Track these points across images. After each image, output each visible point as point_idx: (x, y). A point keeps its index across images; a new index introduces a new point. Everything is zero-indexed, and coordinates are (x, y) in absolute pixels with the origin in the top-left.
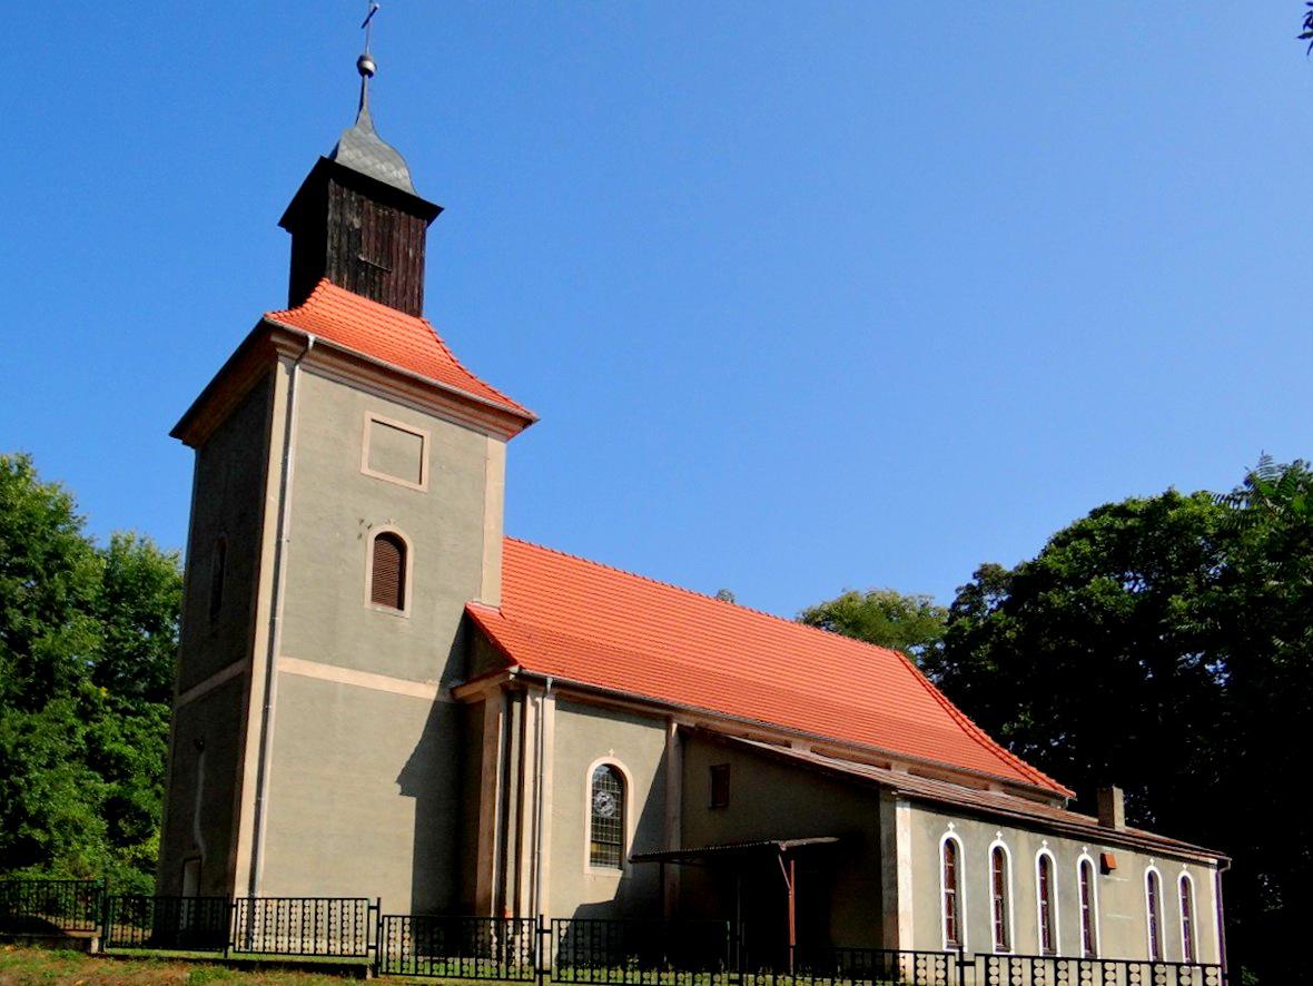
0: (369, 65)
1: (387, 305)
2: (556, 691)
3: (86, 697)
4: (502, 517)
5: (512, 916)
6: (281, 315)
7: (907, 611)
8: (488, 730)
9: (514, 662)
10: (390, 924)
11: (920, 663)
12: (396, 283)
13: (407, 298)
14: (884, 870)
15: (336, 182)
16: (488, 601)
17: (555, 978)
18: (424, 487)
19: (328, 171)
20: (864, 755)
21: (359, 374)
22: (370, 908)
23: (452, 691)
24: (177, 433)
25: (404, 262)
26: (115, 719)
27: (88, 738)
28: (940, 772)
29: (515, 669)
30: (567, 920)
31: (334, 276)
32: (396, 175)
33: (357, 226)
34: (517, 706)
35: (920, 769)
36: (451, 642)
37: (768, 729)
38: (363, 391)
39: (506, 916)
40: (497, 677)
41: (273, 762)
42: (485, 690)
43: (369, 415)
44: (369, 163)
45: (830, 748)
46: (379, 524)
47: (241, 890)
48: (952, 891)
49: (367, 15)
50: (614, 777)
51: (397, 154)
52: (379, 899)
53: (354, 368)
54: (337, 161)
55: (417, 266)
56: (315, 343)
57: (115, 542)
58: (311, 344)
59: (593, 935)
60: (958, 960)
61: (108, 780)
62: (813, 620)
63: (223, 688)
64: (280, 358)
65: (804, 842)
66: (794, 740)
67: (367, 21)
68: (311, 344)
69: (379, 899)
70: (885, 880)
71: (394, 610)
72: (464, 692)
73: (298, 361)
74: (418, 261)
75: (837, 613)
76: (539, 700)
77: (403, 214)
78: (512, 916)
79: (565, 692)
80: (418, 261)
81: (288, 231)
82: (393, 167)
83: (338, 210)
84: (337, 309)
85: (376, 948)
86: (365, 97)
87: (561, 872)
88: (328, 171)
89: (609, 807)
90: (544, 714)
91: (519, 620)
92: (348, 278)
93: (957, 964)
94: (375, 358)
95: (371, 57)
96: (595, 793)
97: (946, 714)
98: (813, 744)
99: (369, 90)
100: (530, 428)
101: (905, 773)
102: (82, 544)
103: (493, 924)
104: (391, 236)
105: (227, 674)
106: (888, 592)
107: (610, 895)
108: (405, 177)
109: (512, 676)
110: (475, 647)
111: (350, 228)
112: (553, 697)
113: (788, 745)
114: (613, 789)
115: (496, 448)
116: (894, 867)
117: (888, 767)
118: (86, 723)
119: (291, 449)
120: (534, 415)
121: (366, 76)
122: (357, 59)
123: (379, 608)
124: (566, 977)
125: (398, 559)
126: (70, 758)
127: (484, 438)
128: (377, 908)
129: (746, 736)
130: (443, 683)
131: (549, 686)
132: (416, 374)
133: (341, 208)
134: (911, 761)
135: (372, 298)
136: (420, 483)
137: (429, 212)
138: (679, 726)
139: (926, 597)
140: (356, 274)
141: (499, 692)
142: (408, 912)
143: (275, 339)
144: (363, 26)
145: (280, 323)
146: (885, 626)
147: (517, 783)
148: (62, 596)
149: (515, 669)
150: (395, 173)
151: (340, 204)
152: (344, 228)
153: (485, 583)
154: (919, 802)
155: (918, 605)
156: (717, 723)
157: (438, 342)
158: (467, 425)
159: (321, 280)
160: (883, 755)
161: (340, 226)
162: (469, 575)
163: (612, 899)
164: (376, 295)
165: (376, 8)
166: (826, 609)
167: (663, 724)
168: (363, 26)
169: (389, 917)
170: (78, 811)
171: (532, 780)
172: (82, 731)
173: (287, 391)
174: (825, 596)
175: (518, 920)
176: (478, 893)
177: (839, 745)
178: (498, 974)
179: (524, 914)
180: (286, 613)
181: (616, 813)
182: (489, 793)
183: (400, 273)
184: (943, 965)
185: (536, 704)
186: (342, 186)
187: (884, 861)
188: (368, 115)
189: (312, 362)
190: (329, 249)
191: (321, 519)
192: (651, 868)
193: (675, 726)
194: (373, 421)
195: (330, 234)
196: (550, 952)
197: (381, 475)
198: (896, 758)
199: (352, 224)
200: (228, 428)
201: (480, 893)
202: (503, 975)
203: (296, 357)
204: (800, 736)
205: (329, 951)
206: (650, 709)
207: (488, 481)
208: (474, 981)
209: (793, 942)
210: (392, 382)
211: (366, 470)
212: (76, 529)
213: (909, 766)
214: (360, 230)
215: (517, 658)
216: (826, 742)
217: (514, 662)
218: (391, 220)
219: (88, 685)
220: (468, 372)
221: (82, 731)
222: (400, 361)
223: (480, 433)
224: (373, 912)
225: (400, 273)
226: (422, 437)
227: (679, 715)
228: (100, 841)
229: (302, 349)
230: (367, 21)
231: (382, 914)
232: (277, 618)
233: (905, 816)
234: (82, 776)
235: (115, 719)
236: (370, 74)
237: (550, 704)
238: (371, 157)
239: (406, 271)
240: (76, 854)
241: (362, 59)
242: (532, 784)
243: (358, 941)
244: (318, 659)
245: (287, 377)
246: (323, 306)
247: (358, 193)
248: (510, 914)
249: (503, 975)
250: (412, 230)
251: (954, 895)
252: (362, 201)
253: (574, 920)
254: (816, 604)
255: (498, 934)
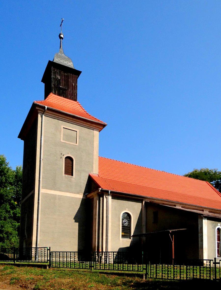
0: (62, 36)
1: (68, 99)
2: (111, 194)
3: (12, 204)
4: (98, 151)
5: (101, 251)
6: (38, 102)
7: (211, 173)
8: (94, 205)
9: (100, 187)
10: (52, 254)
11: (214, 185)
12: (70, 92)
13: (73, 96)
14: (199, 237)
15: (53, 67)
16: (95, 172)
17: (95, 268)
18: (77, 144)
19: (52, 65)
20: (196, 208)
21: (59, 116)
22: (48, 250)
23: (86, 196)
24: (19, 137)
25: (72, 87)
26: (19, 209)
27: (13, 213)
28: (218, 212)
29: (100, 189)
30: (116, 252)
31: (54, 92)
32: (70, 64)
33: (59, 78)
34: (101, 198)
35: (211, 211)
36: (86, 183)
37: (169, 202)
38: (61, 121)
39: (100, 251)
40: (96, 191)
41: (41, 215)
42: (93, 194)
43: (63, 126)
44: (62, 62)
45: (187, 206)
46: (66, 154)
47: (34, 246)
48: (219, 242)
49: (61, 23)
50: (128, 216)
51: (70, 59)
52: (50, 247)
53: (58, 114)
54: (54, 62)
55: (75, 88)
56: (47, 108)
57: (17, 168)
58: (46, 109)
59: (123, 255)
60: (214, 262)
61: (18, 223)
62: (186, 176)
63: (29, 197)
64: (39, 113)
65: (177, 230)
66: (177, 204)
67: (61, 25)
68: (46, 109)
69: (50, 247)
70: (200, 239)
71: (71, 176)
72: (89, 196)
73: (43, 114)
74: (75, 86)
75: (192, 175)
76: (107, 197)
77: (71, 74)
78: (101, 251)
79: (114, 194)
80: (75, 86)
81: (44, 83)
82: (68, 62)
83: (54, 75)
84: (55, 100)
85: (49, 260)
86: (61, 45)
87: (114, 240)
88: (52, 65)
89: (127, 223)
90: (109, 201)
91: (103, 177)
92: (57, 92)
93: (213, 263)
94: (63, 111)
95: (62, 34)
96: (123, 220)
97: (210, 186)
98: (182, 205)
99: (62, 43)
100: (106, 127)
101: (208, 212)
102: (8, 169)
103: (96, 253)
104: (68, 81)
105: (30, 194)
106: (206, 169)
107: (128, 245)
108: (72, 65)
109: (100, 191)
110: (91, 185)
111: (60, 79)
112: (111, 196)
113: (175, 206)
114: (128, 218)
115: (96, 133)
116: (202, 236)
117: (203, 211)
118: (13, 210)
119: (42, 136)
120: (106, 123)
121: (61, 39)
122: (59, 35)
123: (67, 176)
124: (98, 268)
125: (71, 163)
126: (9, 218)
127: (93, 131)
128: (50, 250)
129: (164, 204)
130: (84, 194)
131: (109, 193)
132: (74, 115)
133: (55, 73)
134: (210, 209)
135: (64, 97)
136: (76, 143)
137: (78, 73)
138: (145, 202)
139: (216, 169)
140: (60, 91)
141: (97, 195)
142: (77, 250)
143: (37, 108)
144: (60, 26)
145: (38, 104)
146: (204, 177)
147: (102, 218)
148: (4, 180)
149: (100, 189)
150: (69, 64)
151: (55, 73)
152: (56, 79)
153: (94, 168)
154: (209, 218)
155: (214, 172)
156: (155, 201)
157: (81, 107)
158: (89, 128)
159: (50, 93)
160: (201, 207)
161: (55, 79)
162: (90, 165)
163: (129, 246)
164: (65, 96)
165: (63, 20)
166: (189, 174)
167: (141, 202)
168: (60, 26)
169: (52, 252)
170: (10, 230)
171: (106, 217)
172: (12, 212)
173: (41, 122)
174: (190, 171)
175: (102, 252)
176: (93, 245)
177: (189, 205)
178: (80, 267)
179: (104, 250)
180: (42, 178)
181: (128, 225)
182: (95, 221)
183: (71, 90)
184: (209, 264)
185: (106, 198)
186: (55, 68)
187: (199, 234)
188: (62, 50)
189: (47, 113)
190: (52, 85)
191: (51, 154)
192: (137, 238)
193: (144, 202)
194: (63, 128)
195: (52, 81)
196: (111, 260)
197: (66, 142)
198: (205, 208)
199: (58, 78)
200: (29, 133)
201: (93, 246)
202: (81, 268)
203: (43, 112)
204: (178, 203)
205: (38, 261)
206: (136, 198)
207: (94, 142)
208: (74, 269)
209: (173, 258)
210: (68, 117)
211: (62, 141)
212: (7, 165)
213: (209, 210)
214: (60, 79)
215: (101, 186)
216: (186, 205)
217: (100, 187)
218: (68, 76)
219: (12, 201)
220: (94, 117)
221: (12, 212)
222: (70, 112)
223: (92, 130)
224: (49, 251)
225: (71, 90)
226: (77, 131)
227: (145, 199)
228: (16, 236)
229: (44, 110)
230: (61, 25)
231: (51, 251)
232: (40, 179)
233: (205, 222)
234: (12, 222)
235: (19, 209)
236: (62, 38)
237: (110, 198)
238: (63, 60)
239: (72, 89)
240: (11, 239)
241: (60, 34)
242: (106, 218)
243: (39, 257)
244: (51, 189)
245: (41, 118)
246: (51, 100)
247: (59, 70)
248: (101, 251)
249: (81, 268)
250: (74, 78)
251: (220, 243)
252: (60, 72)
253: (118, 252)
254: (187, 173)
255: (98, 255)
